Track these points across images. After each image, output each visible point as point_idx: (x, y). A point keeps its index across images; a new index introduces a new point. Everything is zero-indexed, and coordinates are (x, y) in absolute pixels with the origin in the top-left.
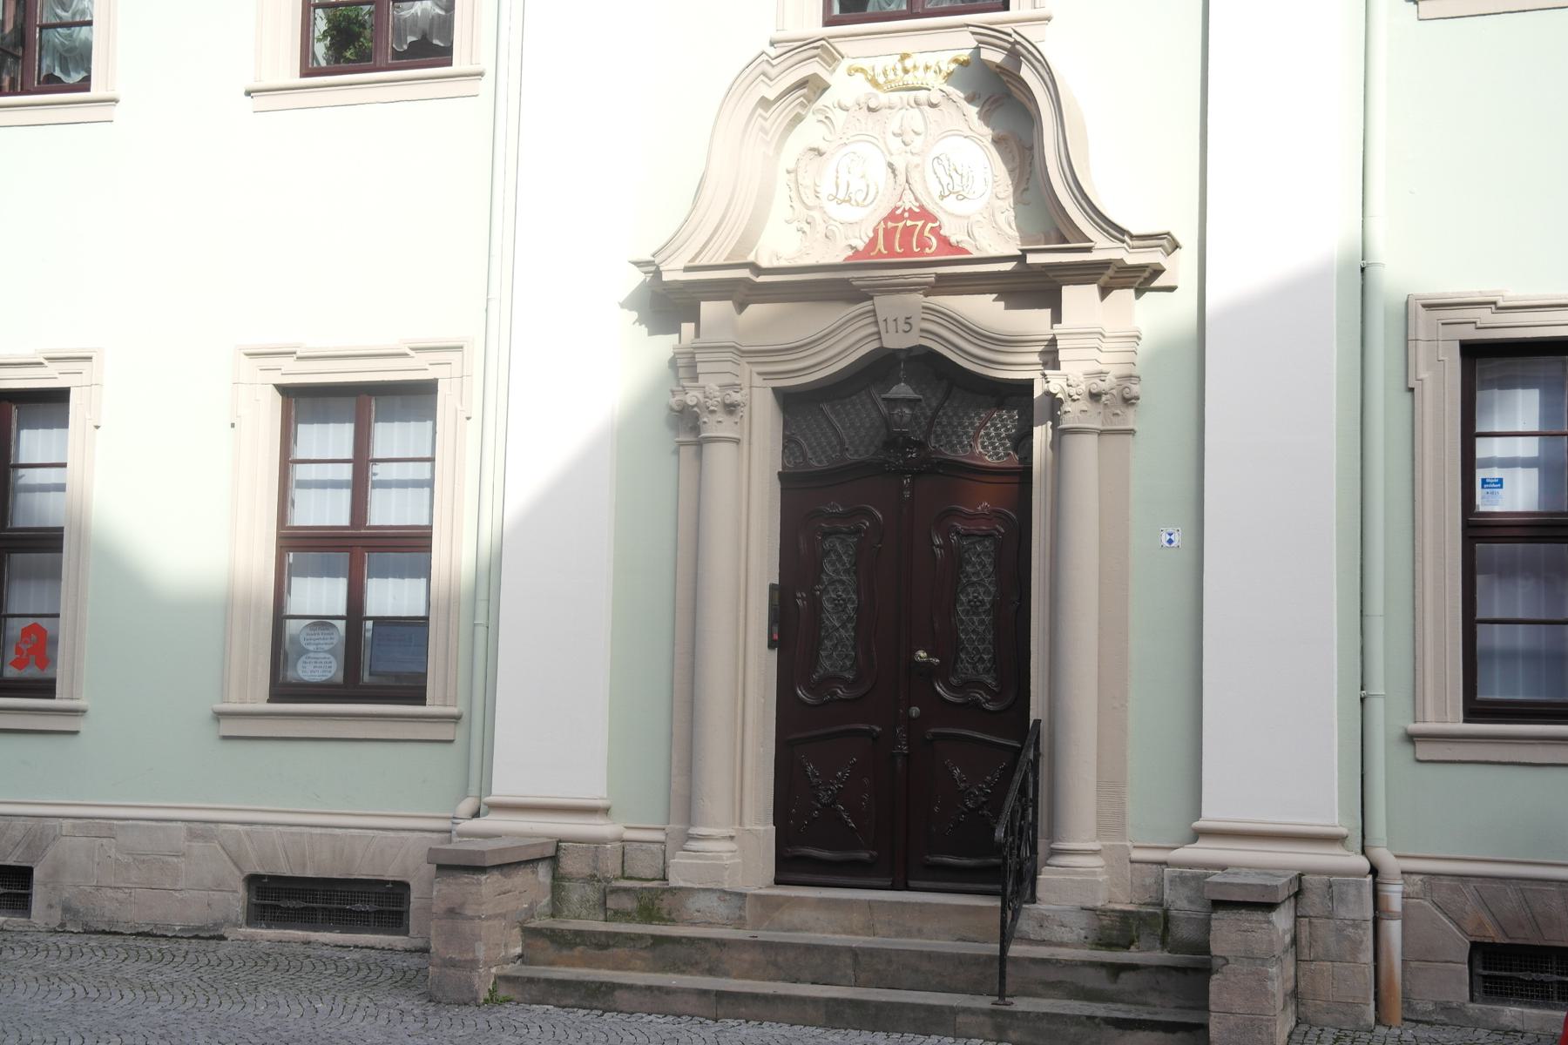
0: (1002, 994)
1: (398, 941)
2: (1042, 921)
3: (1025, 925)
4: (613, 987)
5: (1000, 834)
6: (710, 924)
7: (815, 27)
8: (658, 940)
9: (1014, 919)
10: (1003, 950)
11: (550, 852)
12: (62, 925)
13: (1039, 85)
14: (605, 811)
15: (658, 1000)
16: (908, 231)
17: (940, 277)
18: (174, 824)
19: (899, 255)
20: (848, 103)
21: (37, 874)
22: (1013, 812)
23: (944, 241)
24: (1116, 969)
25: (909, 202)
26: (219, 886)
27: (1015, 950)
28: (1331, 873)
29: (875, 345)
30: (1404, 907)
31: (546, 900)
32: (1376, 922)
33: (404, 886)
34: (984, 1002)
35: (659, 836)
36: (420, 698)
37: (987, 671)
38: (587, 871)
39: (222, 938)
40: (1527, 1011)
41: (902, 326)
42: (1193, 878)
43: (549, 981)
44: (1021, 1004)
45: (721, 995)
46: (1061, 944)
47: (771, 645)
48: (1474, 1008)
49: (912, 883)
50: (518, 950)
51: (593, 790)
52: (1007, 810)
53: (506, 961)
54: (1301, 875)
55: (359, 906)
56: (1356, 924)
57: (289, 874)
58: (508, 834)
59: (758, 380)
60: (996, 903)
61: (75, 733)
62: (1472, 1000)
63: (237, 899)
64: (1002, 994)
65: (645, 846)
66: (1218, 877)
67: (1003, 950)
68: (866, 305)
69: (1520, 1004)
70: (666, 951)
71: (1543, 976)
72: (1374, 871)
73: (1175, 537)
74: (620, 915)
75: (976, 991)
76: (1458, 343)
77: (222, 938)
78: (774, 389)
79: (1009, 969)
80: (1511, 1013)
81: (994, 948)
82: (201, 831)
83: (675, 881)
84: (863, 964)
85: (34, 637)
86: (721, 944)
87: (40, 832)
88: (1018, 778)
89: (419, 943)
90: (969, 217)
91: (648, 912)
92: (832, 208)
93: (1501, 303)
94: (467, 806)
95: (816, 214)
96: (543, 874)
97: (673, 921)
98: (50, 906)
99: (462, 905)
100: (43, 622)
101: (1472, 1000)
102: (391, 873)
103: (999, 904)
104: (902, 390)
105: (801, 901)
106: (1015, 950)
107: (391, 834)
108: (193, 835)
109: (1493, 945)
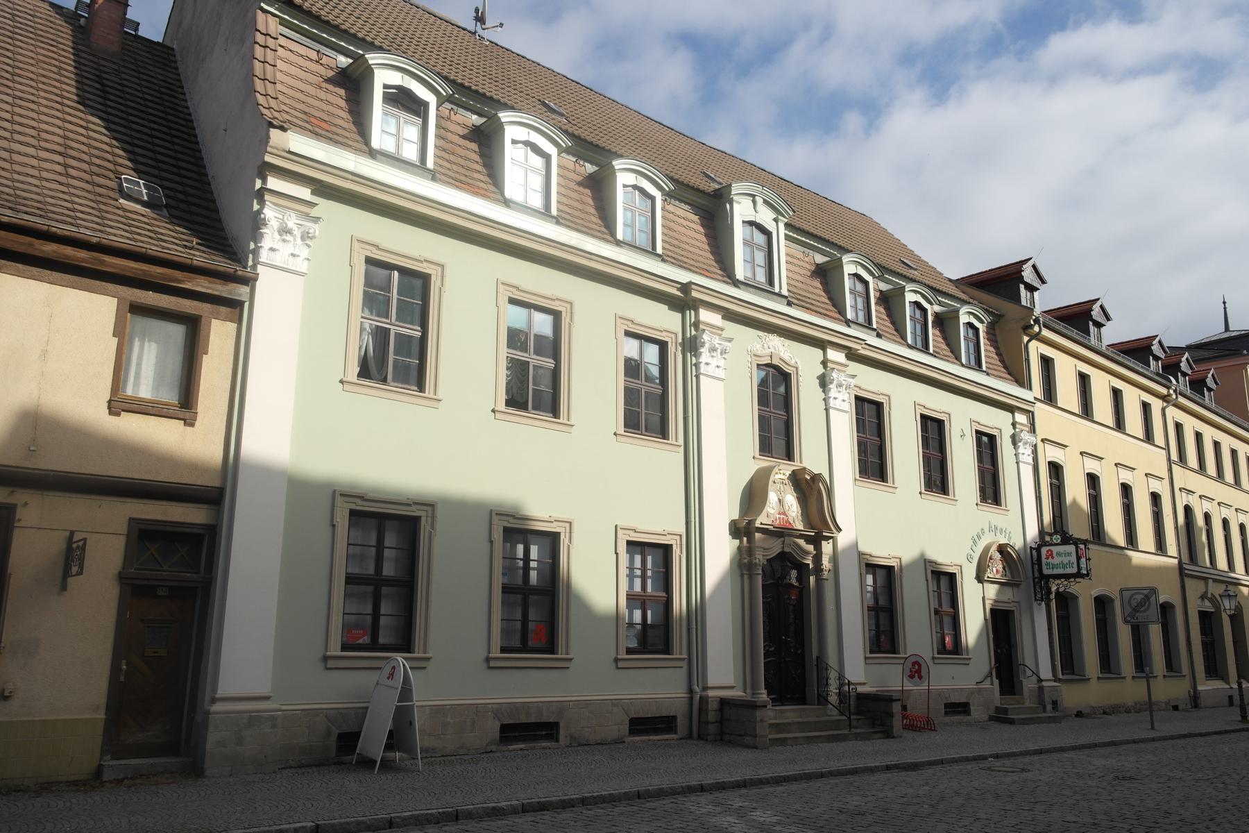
1: (675, 736)
4: (786, 739)
12: (571, 744)
13: (421, 400)
14: (267, 698)
17: (801, 534)
33: (674, 717)
39: (624, 742)
51: (265, 690)
55: (660, 726)
57: (643, 716)
61: (968, 664)
65: (453, 707)
76: (348, 510)
77: (624, 742)
82: (615, 703)
87: (562, 707)
98: (566, 737)
105: (787, 710)
107: (672, 700)
108: (613, 704)
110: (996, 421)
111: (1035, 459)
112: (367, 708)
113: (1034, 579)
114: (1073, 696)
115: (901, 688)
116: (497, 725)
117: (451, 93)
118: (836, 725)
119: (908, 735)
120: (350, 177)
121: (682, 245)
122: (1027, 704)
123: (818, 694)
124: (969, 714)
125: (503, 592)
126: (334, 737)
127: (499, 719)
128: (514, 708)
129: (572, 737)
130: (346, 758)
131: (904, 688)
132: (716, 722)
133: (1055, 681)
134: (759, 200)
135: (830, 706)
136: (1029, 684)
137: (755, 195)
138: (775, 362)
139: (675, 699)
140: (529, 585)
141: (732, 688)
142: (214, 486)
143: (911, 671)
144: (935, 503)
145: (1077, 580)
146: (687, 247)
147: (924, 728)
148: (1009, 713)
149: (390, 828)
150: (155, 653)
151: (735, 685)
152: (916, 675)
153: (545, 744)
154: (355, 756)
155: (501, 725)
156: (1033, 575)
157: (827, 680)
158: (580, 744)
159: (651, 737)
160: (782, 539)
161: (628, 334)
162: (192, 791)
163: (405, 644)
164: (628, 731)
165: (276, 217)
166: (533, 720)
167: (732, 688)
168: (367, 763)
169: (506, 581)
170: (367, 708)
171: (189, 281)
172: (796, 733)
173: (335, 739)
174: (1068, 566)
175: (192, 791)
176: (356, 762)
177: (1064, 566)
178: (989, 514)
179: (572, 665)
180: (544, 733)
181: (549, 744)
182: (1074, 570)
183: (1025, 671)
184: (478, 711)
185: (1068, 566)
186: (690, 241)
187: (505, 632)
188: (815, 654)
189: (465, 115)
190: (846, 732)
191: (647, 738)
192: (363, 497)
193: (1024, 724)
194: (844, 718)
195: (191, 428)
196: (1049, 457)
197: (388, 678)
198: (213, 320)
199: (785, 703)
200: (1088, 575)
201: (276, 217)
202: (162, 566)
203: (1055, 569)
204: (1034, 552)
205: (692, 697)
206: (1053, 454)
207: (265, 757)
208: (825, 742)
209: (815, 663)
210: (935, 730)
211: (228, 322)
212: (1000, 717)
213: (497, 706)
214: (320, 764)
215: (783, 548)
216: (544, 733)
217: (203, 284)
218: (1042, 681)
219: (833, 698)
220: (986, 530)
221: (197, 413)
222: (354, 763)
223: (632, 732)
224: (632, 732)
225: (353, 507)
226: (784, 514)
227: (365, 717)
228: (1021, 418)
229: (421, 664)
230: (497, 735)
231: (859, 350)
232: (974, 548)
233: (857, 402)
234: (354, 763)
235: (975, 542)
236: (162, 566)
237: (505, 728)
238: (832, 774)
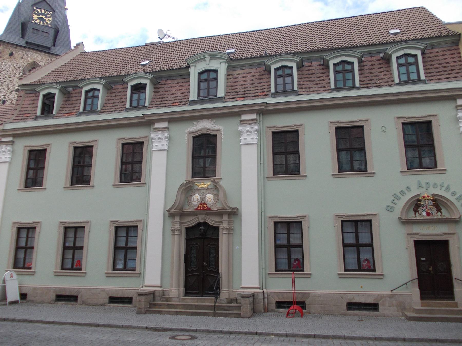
0: (215, 311)
1: (131, 305)
2: (220, 300)
3: (218, 301)
4: (162, 311)
5: (214, 288)
6: (176, 302)
7: (190, 179)
8: (168, 304)
9: (217, 300)
10: (215, 304)
11: (153, 292)
15: (168, 313)
16: (203, 206)
18: (142, 282)
19: (202, 209)
20: (195, 189)
21: (79, 297)
22: (216, 285)
23: (208, 207)
24: (230, 306)
25: (203, 202)
26: (105, 298)
27: (216, 304)
28: (258, 292)
29: (199, 221)
30: (267, 297)
31: (152, 299)
32: (264, 299)
34: (212, 311)
35: (169, 290)
36: (135, 270)
37: (214, 266)
38: (158, 295)
40: (283, 310)
41: (202, 219)
42: (239, 293)
43: (153, 311)
44: (217, 312)
45: (177, 312)
46: (223, 303)
47: (184, 262)
48: (276, 310)
49: (203, 295)
50: (149, 306)
52: (215, 285)
53: (147, 308)
54: (254, 293)
56: (261, 299)
58: (148, 290)
59: (183, 226)
60: (214, 298)
62: (276, 309)
63: (107, 300)
64: (215, 311)
66: (243, 293)
67: (215, 304)
68: (196, 216)
69: (282, 309)
70: (169, 306)
71: (284, 305)
72: (263, 292)
73: (238, 248)
74: (163, 301)
75: (211, 310)
78: (185, 227)
79: (216, 307)
80: (281, 310)
81: (214, 304)
82: (103, 290)
83: (171, 296)
84: (196, 307)
85: (79, 262)
86: (177, 305)
87: (79, 290)
88: (217, 281)
89: (134, 306)
90: (210, 204)
91: (167, 301)
92: (193, 203)
93: (31, 146)
94: (141, 286)
95: (190, 203)
96: (152, 296)
97: (170, 302)
99: (141, 300)
100: (80, 260)
101: (276, 309)
102: (130, 296)
103: (214, 298)
104: (202, 228)
105: (188, 299)
106: (216, 304)
109: (279, 301)
115: (292, 291)
124: (378, 311)
139: (132, 290)
140: (359, 243)
153: (73, 303)
172: (447, 314)
180: (73, 299)
184: (48, 289)
197: (11, 277)
199: (204, 296)
208: (190, 315)
214: (50, 303)
216: (73, 299)
233: (140, 178)
238: (339, 338)
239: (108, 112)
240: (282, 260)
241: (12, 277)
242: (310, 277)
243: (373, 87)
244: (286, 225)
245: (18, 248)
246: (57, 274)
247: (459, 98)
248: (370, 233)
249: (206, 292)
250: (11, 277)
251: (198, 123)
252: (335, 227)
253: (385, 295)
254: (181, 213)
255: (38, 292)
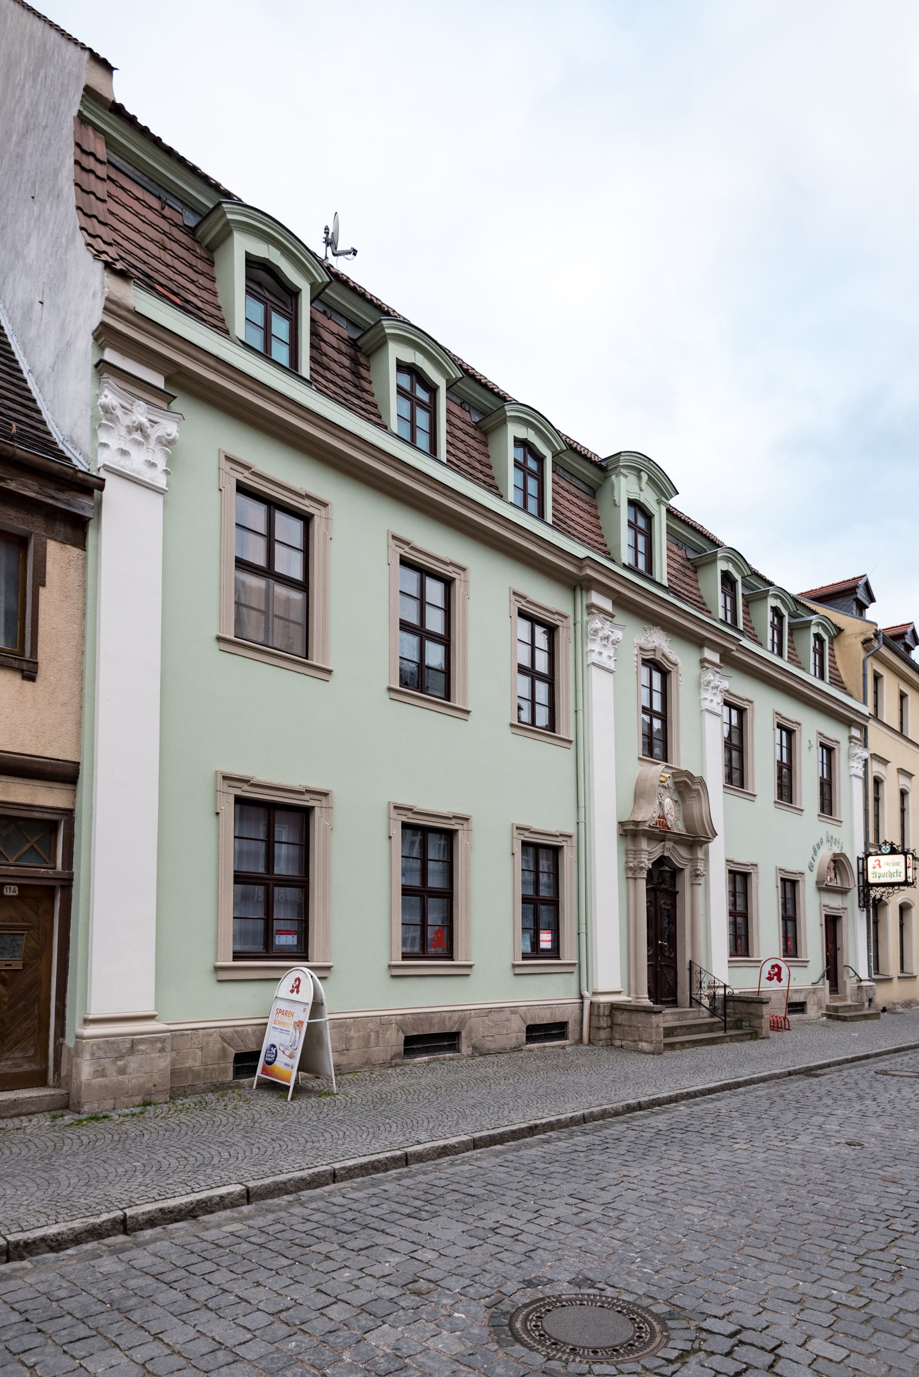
14: (151, 1018)
21: (463, 1034)
61: (806, 967)
82: (514, 1010)
87: (464, 1017)
110: (835, 732)
111: (866, 773)
112: (266, 1024)
113: (859, 887)
114: (884, 995)
115: (757, 990)
116: (402, 1037)
117: (328, 280)
118: (711, 1027)
119: (772, 1034)
120: (212, 362)
121: (567, 521)
122: (849, 1002)
123: (691, 998)
125: (403, 895)
126: (231, 1059)
127: (403, 1031)
128: (419, 1018)
129: (474, 1047)
130: (245, 1081)
131: (761, 990)
132: (608, 1027)
133: (869, 980)
134: (644, 477)
135: (703, 1009)
136: (849, 984)
137: (641, 470)
138: (658, 657)
141: (619, 993)
142: (66, 759)
143: (770, 973)
144: (784, 815)
145: (902, 888)
146: (572, 523)
147: (781, 1028)
148: (840, 1011)
149: (334, 1182)
150: (6, 965)
151: (621, 990)
152: (775, 977)
154: (256, 1078)
155: (406, 1037)
156: (859, 883)
157: (701, 983)
158: (479, 1051)
159: (546, 1044)
160: (662, 843)
161: (522, 614)
162: (71, 1136)
163: (302, 953)
164: (525, 1038)
165: (123, 407)
166: (435, 1030)
167: (619, 993)
168: (274, 1087)
169: (404, 883)
170: (266, 1024)
171: (11, 480)
173: (232, 1060)
174: (895, 875)
175: (71, 1136)
176: (258, 1085)
177: (891, 875)
178: (825, 828)
179: (473, 972)
180: (446, 1043)
181: (452, 1055)
182: (902, 879)
183: (848, 972)
184: (383, 1023)
185: (895, 875)
186: (574, 517)
187: (239, 935)
188: (688, 957)
189: (340, 323)
190: (721, 1034)
191: (542, 1044)
192: (249, 781)
193: (853, 1021)
194: (717, 1019)
195: (31, 683)
196: (439, 857)
197: (292, 991)
198: (48, 541)
200: (913, 883)
201: (123, 407)
202: (7, 860)
203: (881, 878)
204: (861, 861)
205: (582, 1003)
206: (875, 768)
207: (154, 1086)
209: (687, 966)
210: (789, 1029)
211: (67, 546)
212: (834, 1015)
213: (399, 1018)
214: (219, 1088)
215: (663, 852)
216: (446, 1043)
217: (31, 486)
218: (861, 980)
219: (706, 1002)
220: (824, 840)
221: (37, 663)
222: (254, 1087)
223: (530, 1039)
224: (530, 1039)
225: (239, 792)
226: (664, 818)
227: (264, 1035)
228: (856, 733)
229: (324, 971)
230: (402, 1048)
231: (733, 650)
232: (815, 857)
234: (254, 1087)
235: (815, 852)
236: (7, 860)
237: (409, 1040)
239: (699, 608)
240: (288, 926)
241: (298, 992)
242: (468, 975)
243: (369, 420)
244: (262, 812)
245: (447, 895)
246: (396, 974)
247: (709, 648)
248: (419, 861)
249: (664, 999)
250: (292, 991)
251: (652, 631)
252: (218, 814)
253: (421, 1016)
254: (632, 830)
255: (352, 1033)
